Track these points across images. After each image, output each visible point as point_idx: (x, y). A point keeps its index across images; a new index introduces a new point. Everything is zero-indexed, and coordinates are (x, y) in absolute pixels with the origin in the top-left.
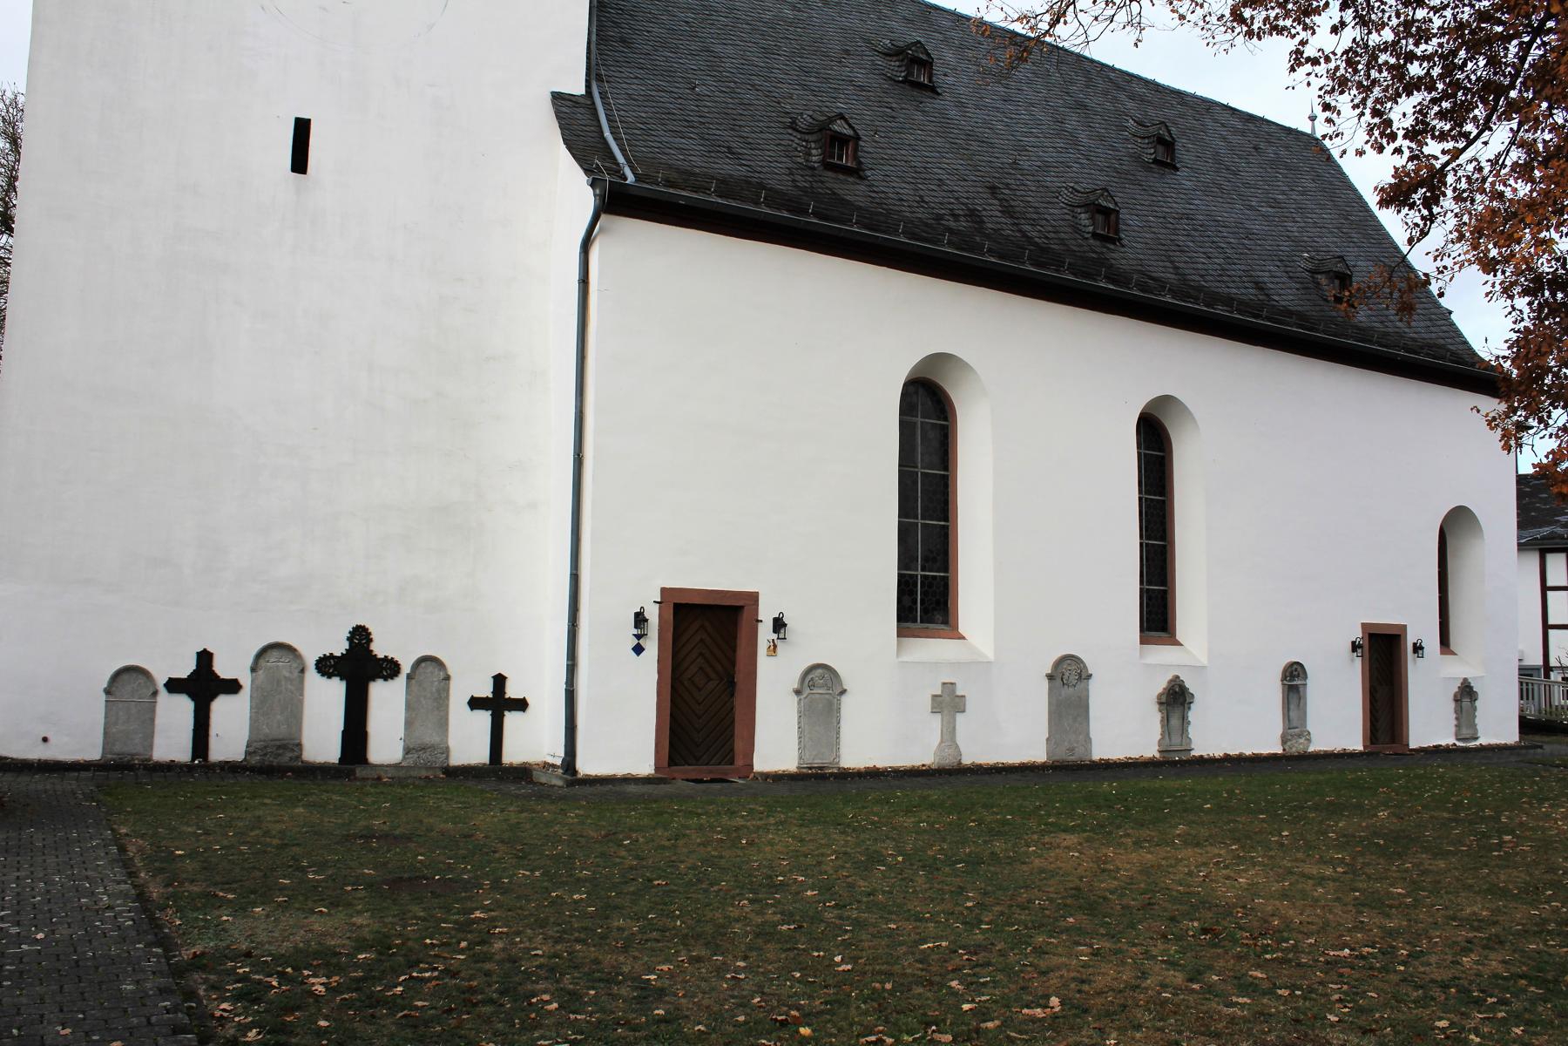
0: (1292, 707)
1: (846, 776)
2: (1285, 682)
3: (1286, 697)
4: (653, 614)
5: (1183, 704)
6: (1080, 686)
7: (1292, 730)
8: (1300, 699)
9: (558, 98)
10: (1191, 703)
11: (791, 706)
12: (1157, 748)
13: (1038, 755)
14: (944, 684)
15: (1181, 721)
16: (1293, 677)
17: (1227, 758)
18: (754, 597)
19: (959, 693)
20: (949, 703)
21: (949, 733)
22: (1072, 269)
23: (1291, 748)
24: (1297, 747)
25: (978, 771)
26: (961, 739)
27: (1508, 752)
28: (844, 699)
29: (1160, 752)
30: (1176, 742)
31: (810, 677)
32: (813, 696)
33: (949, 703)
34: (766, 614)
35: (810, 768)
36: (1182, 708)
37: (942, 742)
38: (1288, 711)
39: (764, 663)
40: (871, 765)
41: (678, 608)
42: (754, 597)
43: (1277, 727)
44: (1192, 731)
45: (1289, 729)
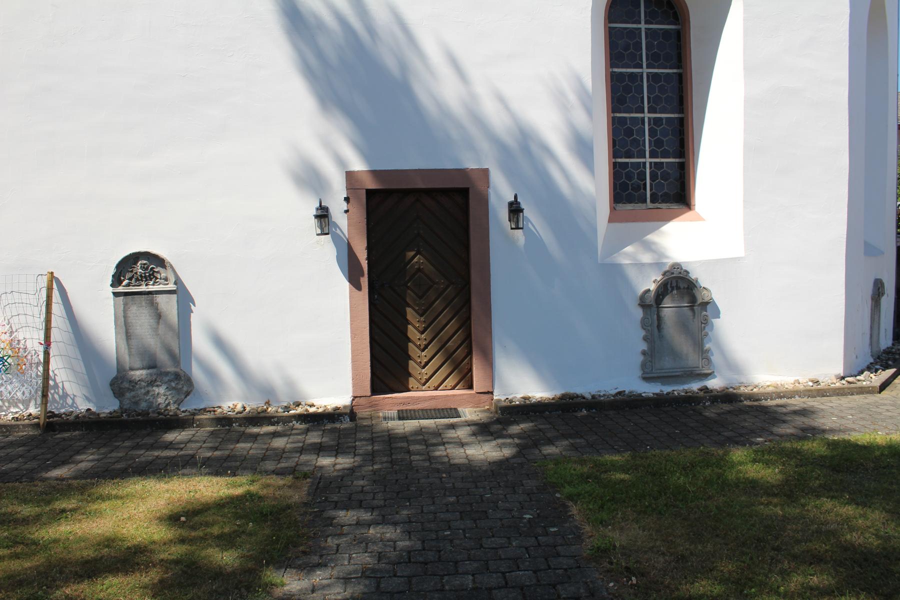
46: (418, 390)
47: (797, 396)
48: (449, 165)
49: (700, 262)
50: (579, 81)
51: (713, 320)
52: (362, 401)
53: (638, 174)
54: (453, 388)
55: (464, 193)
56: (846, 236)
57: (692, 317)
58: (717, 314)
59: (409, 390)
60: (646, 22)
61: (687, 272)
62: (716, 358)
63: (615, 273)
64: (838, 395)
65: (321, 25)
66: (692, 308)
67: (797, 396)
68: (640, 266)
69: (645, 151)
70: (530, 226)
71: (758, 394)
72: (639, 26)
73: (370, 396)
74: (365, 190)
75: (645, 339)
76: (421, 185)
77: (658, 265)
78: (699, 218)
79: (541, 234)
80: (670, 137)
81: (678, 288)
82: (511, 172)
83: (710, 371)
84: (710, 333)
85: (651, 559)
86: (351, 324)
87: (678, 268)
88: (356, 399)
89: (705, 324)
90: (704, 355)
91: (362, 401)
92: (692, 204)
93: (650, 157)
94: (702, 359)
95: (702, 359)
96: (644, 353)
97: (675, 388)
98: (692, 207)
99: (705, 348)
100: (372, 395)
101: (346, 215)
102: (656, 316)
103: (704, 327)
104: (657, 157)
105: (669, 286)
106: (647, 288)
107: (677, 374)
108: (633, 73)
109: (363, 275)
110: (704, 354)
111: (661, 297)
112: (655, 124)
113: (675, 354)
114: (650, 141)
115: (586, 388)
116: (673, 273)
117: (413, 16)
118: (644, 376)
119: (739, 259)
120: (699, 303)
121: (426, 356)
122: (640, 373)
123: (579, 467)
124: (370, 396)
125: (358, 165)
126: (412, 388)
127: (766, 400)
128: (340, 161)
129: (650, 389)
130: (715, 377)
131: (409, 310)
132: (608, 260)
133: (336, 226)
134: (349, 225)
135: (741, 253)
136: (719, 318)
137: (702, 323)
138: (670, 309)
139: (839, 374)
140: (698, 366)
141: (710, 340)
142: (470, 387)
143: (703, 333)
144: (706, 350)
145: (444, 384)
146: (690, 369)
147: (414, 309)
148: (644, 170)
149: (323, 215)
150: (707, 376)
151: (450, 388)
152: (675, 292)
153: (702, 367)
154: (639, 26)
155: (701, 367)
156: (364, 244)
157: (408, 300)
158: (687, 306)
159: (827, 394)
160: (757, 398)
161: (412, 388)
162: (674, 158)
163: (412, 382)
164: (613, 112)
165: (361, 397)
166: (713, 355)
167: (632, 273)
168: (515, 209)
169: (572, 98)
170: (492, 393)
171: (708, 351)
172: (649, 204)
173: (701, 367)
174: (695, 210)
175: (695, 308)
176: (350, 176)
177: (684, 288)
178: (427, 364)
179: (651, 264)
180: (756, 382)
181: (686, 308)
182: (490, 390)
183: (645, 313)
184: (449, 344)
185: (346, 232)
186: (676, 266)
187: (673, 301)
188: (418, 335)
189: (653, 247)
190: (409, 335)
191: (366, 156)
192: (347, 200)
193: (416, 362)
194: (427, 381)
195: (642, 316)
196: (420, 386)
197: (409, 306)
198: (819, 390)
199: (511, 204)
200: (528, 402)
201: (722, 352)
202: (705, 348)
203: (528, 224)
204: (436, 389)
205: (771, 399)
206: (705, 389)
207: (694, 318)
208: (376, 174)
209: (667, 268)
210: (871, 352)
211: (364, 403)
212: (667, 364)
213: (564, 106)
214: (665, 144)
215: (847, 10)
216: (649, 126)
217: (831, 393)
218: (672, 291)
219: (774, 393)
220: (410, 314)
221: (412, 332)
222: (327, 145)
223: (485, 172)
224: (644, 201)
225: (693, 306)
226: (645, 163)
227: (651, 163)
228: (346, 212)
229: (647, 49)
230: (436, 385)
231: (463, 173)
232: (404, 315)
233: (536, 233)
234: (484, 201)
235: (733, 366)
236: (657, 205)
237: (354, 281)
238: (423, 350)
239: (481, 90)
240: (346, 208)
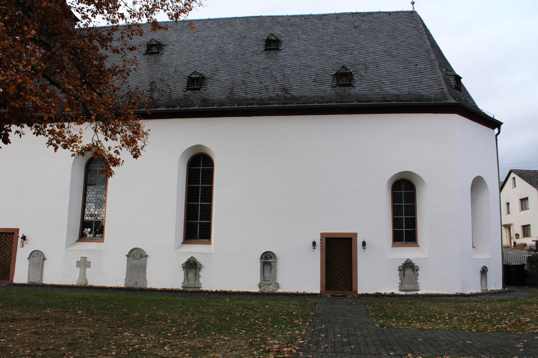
0: (266, 271)
1: (202, 292)
2: (262, 260)
3: (262, 267)
4: (318, 242)
5: (196, 268)
6: (142, 259)
7: (266, 282)
8: (272, 268)
9: (462, 78)
10: (201, 268)
11: (27, 262)
12: (182, 285)
13: (121, 284)
14: (81, 257)
15: (194, 275)
16: (266, 258)
17: (216, 292)
18: (355, 235)
19: (88, 261)
20: (84, 264)
21: (83, 274)
22: (257, 104)
23: (264, 290)
24: (270, 289)
25: (92, 288)
26: (88, 277)
27: (284, 297)
28: (45, 261)
29: (183, 287)
30: (192, 283)
31: (32, 255)
32: (33, 260)
33: (84, 264)
34: (20, 235)
35: (31, 283)
36: (195, 270)
37: (80, 277)
38: (264, 273)
39: (20, 251)
40: (111, 286)
41: (327, 239)
42: (355, 235)
43: (257, 279)
44: (201, 280)
45: (264, 281)
60: (404, 190)
61: (412, 261)
66: (413, 271)
75: (400, 279)
85: (314, 327)
96: (400, 283)
118: (183, 286)
122: (399, 289)
129: (403, 293)
150: (418, 290)
164: (188, 184)
172: (404, 242)
183: (400, 272)
199: (363, 242)
206: (417, 293)
224: (403, 241)
226: (403, 230)
229: (402, 197)
236: (407, 242)
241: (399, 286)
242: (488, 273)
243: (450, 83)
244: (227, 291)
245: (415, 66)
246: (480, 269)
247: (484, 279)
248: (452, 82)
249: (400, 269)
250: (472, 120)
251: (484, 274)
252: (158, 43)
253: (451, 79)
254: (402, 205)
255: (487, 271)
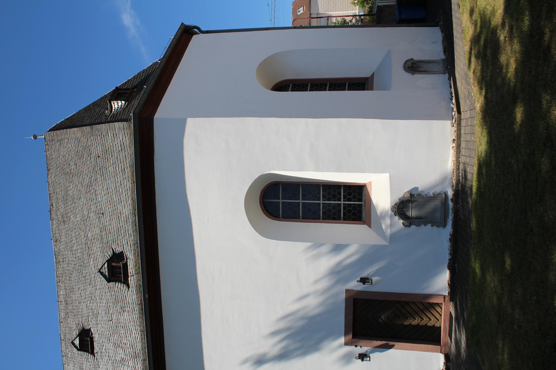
46: (441, 323)
47: (459, 160)
48: (344, 305)
49: (391, 197)
50: (308, 248)
51: (419, 190)
52: (443, 349)
53: (348, 207)
54: (441, 308)
55: (355, 299)
56: (381, 120)
57: (417, 202)
58: (416, 188)
59: (441, 327)
61: (396, 204)
62: (438, 190)
63: (394, 238)
64: (460, 137)
65: (285, 347)
66: (412, 202)
67: (459, 160)
68: (391, 225)
69: (338, 204)
70: (371, 274)
71: (456, 180)
72: (281, 202)
73: (441, 346)
74: (353, 339)
75: (425, 225)
76: (351, 317)
77: (391, 217)
78: (370, 183)
79: (374, 270)
80: (331, 190)
81: (403, 208)
82: (347, 280)
83: (444, 195)
84: (425, 193)
86: (409, 350)
87: (393, 209)
88: (442, 352)
89: (421, 196)
90: (436, 196)
91: (443, 349)
92: (363, 185)
93: (341, 201)
94: (438, 197)
95: (438, 197)
96: (432, 226)
97: (451, 214)
98: (365, 185)
99: (433, 196)
100: (441, 345)
101: (362, 347)
102: (415, 220)
103: (422, 196)
104: (341, 197)
105: (402, 213)
106: (402, 224)
107: (444, 211)
108: (302, 207)
109: (388, 344)
110: (435, 196)
111: (406, 217)
112: (325, 198)
113: (434, 211)
114: (333, 201)
115: (446, 257)
116: (396, 211)
117: (281, 313)
118: (443, 225)
119: (390, 176)
120: (410, 199)
121: (426, 319)
123: (505, 31)
124: (441, 346)
125: (342, 340)
126: (439, 325)
127: (459, 176)
128: (340, 346)
130: (447, 191)
131: (405, 323)
132: (388, 239)
133: (367, 351)
134: (367, 347)
135: (387, 175)
136: (418, 188)
137: (420, 197)
138: (412, 213)
139: (451, 123)
140: (441, 200)
141: (429, 193)
142: (442, 304)
143: (424, 197)
144: (433, 195)
145: (439, 312)
146: (442, 204)
147: (404, 322)
148: (347, 204)
149: (362, 357)
150: (446, 196)
151: (441, 309)
152: (404, 210)
153: (442, 198)
154: (281, 202)
155: (441, 198)
156: (375, 342)
157: (401, 323)
158: (412, 204)
159: (459, 144)
160: (458, 180)
161: (439, 325)
162: (341, 189)
163: (437, 325)
165: (441, 350)
166: (436, 192)
167: (395, 229)
168: (364, 280)
169: (315, 252)
170: (445, 296)
171: (434, 194)
173: (441, 198)
174: (366, 183)
175: (413, 200)
176: (346, 344)
177: (403, 205)
178: (429, 318)
179: (391, 221)
180: (451, 171)
181: (413, 205)
182: (443, 296)
183: (413, 225)
184: (421, 308)
185: (369, 348)
186: (393, 208)
187: (408, 211)
188: (416, 321)
189: (383, 215)
190: (416, 324)
191: (339, 337)
192: (356, 346)
193: (428, 323)
194: (437, 319)
195: (414, 226)
196: (439, 322)
197: (403, 323)
198: (457, 139)
200: (452, 250)
201: (436, 186)
202: (433, 196)
203: (370, 275)
204: (441, 315)
205: (459, 173)
207: (418, 201)
208: (346, 334)
209: (393, 213)
210: (442, 74)
211: (444, 349)
212: (438, 215)
213: (318, 256)
214: (335, 193)
215: (273, 119)
216: (326, 201)
217: (459, 141)
218: (404, 211)
219: (456, 172)
220: (406, 323)
221: (415, 322)
222: (333, 350)
223: (347, 291)
224: (361, 205)
225: (412, 201)
226: (344, 204)
227: (344, 201)
228: (361, 347)
230: (439, 315)
231: (347, 300)
232: (407, 326)
233: (374, 272)
234: (359, 292)
235: (443, 180)
237: (391, 347)
238: (423, 319)
239: (312, 289)
240: (360, 347)
241: (438, 226)
242: (416, 58)
243: (121, 107)
244: (450, 260)
245: (100, 157)
246: (408, 76)
247: (425, 67)
248: (120, 104)
249: (408, 224)
250: (160, 282)
251: (419, 67)
252: (106, 261)
253: (116, 106)
254: (302, 203)
255: (412, 59)
